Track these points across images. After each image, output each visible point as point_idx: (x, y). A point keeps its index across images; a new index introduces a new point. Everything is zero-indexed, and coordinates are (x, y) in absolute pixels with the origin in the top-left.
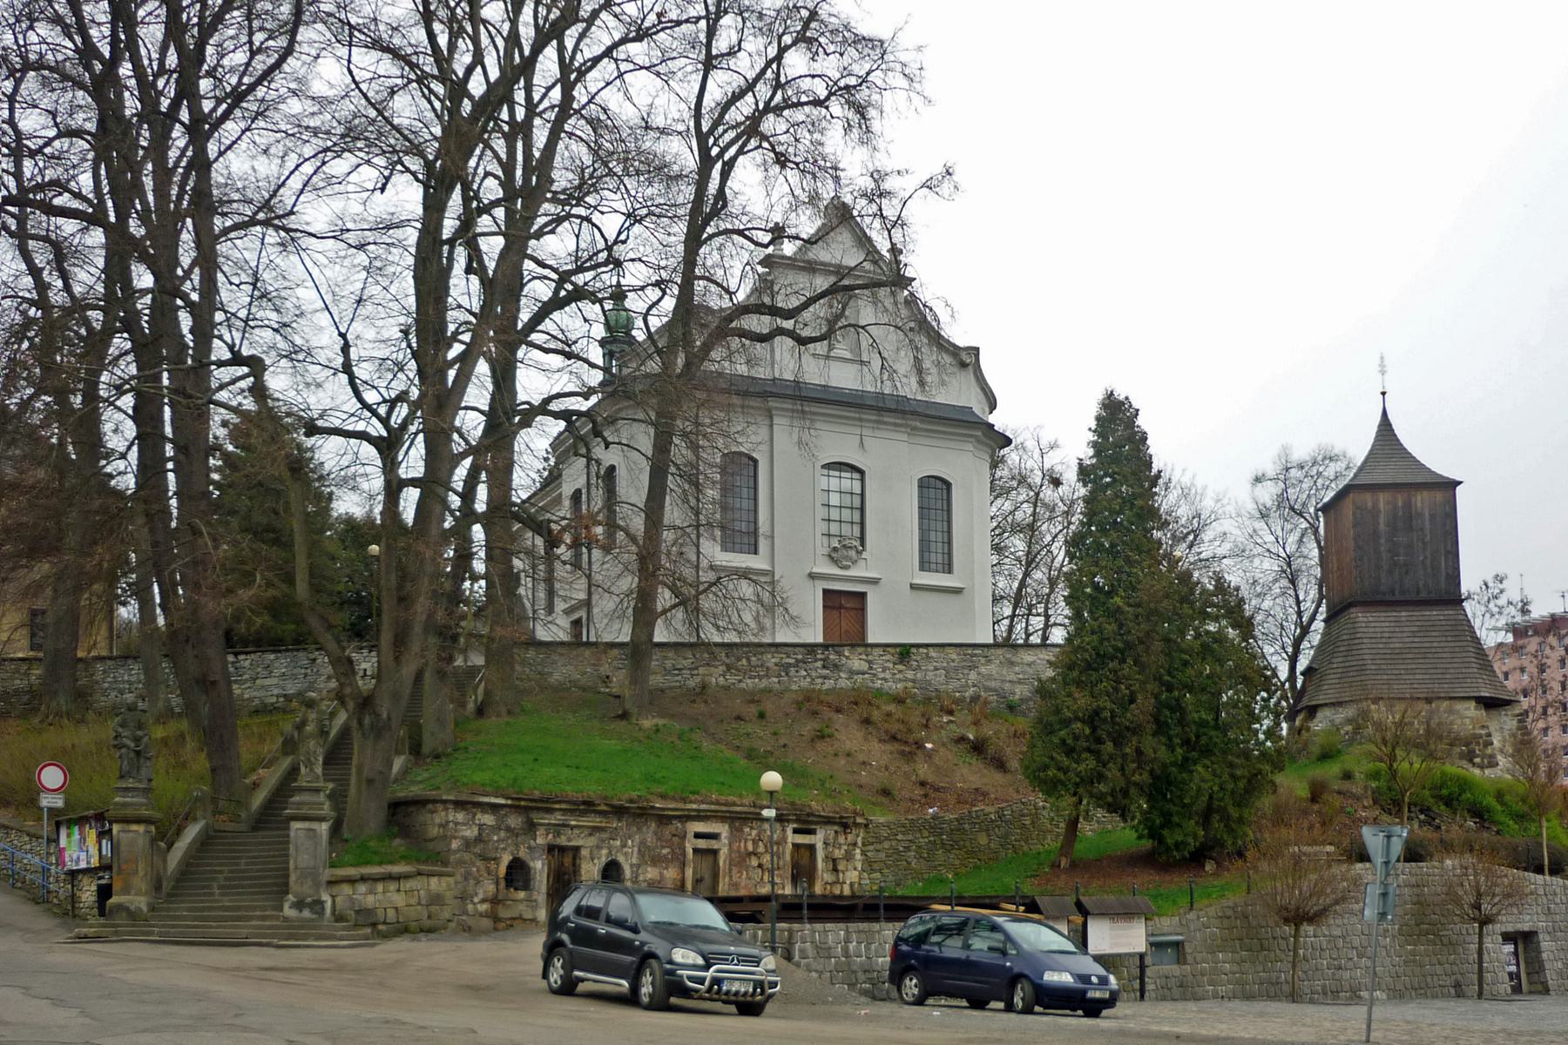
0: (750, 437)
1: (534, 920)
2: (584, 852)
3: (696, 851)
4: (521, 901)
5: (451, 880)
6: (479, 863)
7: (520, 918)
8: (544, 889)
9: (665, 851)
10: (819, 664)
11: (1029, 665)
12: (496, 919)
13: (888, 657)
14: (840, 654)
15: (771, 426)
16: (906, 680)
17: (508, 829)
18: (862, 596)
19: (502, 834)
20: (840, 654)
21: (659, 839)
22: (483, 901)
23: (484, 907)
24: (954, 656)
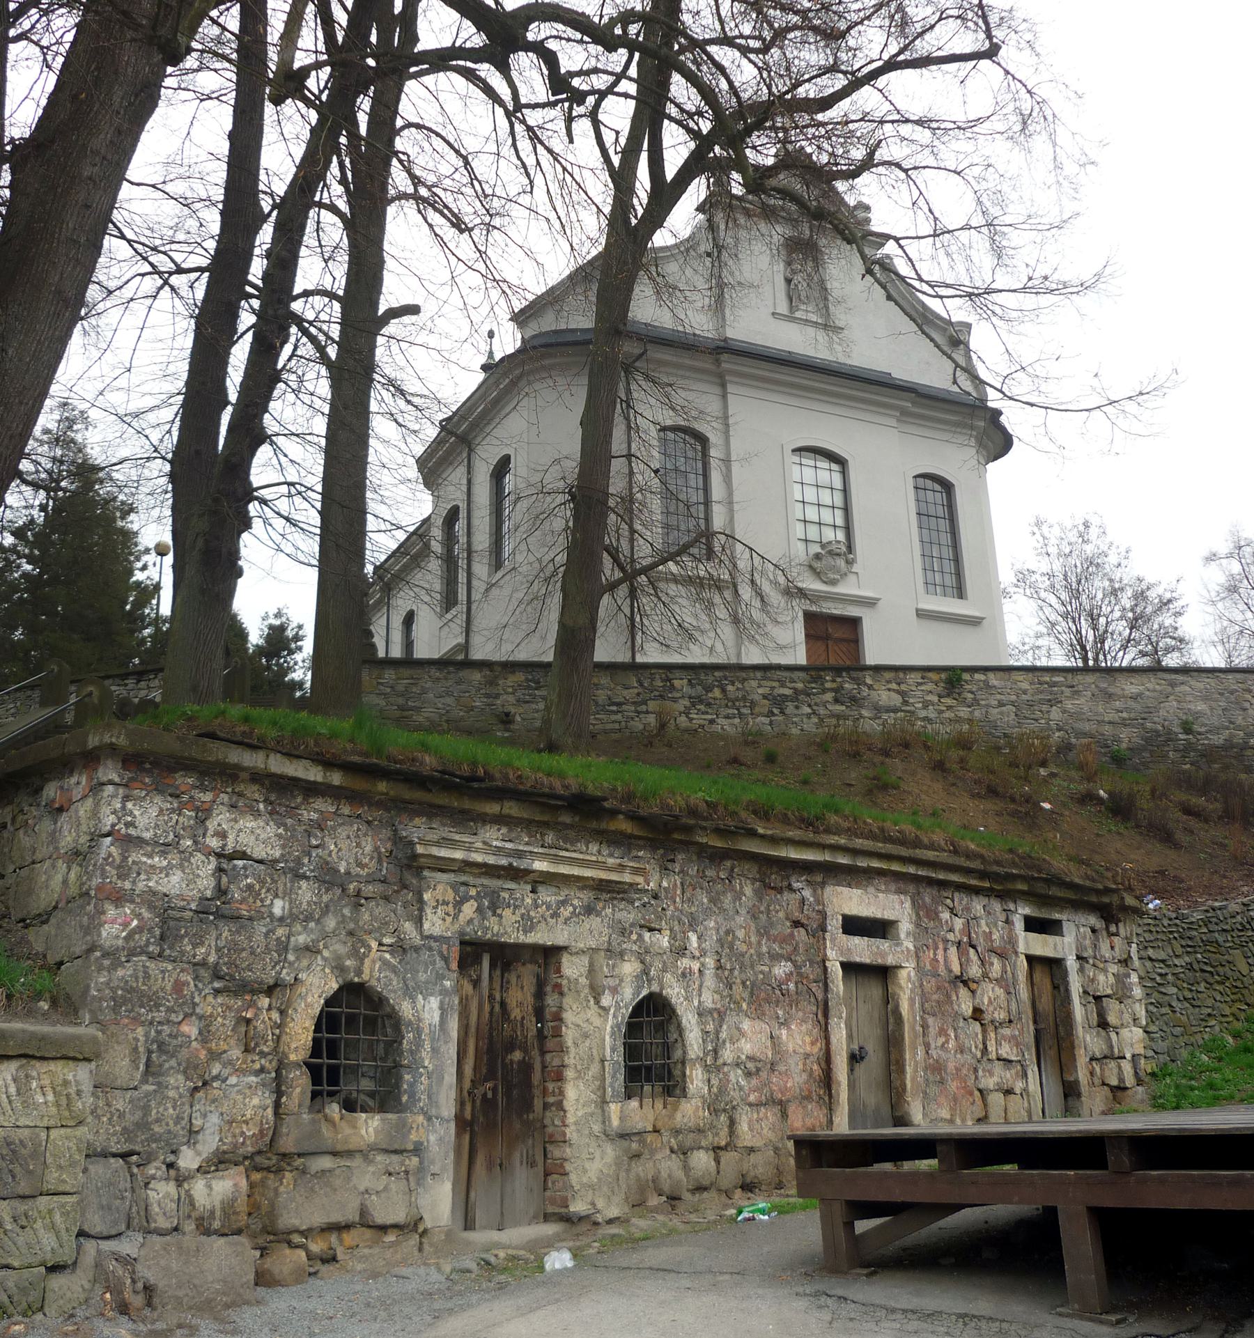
0: (698, 400)
1: (412, 1227)
2: (572, 968)
3: (849, 968)
4: (366, 1153)
5: (81, 1074)
6: (209, 1005)
7: (365, 1222)
8: (447, 1105)
9: (781, 970)
10: (829, 696)
11: (1134, 698)
12: (267, 1233)
13: (930, 687)
14: (859, 682)
15: (724, 396)
16: (958, 720)
17: (328, 877)
18: (855, 623)
19: (306, 893)
20: (859, 682)
21: (763, 932)
22: (219, 1162)
23: (216, 1191)
24: (1025, 686)
